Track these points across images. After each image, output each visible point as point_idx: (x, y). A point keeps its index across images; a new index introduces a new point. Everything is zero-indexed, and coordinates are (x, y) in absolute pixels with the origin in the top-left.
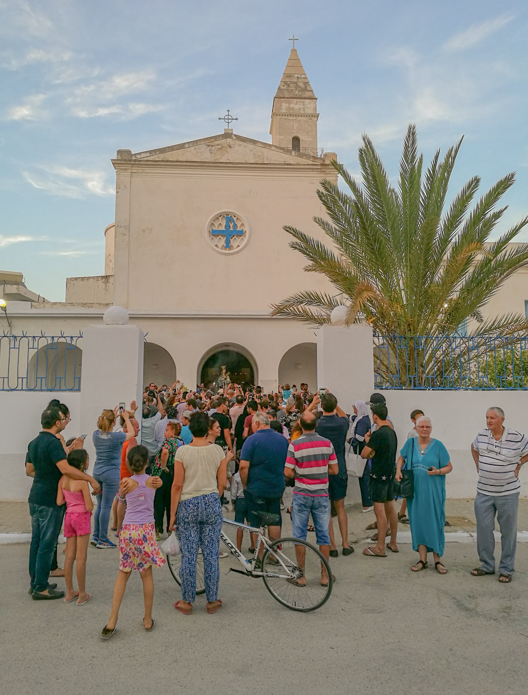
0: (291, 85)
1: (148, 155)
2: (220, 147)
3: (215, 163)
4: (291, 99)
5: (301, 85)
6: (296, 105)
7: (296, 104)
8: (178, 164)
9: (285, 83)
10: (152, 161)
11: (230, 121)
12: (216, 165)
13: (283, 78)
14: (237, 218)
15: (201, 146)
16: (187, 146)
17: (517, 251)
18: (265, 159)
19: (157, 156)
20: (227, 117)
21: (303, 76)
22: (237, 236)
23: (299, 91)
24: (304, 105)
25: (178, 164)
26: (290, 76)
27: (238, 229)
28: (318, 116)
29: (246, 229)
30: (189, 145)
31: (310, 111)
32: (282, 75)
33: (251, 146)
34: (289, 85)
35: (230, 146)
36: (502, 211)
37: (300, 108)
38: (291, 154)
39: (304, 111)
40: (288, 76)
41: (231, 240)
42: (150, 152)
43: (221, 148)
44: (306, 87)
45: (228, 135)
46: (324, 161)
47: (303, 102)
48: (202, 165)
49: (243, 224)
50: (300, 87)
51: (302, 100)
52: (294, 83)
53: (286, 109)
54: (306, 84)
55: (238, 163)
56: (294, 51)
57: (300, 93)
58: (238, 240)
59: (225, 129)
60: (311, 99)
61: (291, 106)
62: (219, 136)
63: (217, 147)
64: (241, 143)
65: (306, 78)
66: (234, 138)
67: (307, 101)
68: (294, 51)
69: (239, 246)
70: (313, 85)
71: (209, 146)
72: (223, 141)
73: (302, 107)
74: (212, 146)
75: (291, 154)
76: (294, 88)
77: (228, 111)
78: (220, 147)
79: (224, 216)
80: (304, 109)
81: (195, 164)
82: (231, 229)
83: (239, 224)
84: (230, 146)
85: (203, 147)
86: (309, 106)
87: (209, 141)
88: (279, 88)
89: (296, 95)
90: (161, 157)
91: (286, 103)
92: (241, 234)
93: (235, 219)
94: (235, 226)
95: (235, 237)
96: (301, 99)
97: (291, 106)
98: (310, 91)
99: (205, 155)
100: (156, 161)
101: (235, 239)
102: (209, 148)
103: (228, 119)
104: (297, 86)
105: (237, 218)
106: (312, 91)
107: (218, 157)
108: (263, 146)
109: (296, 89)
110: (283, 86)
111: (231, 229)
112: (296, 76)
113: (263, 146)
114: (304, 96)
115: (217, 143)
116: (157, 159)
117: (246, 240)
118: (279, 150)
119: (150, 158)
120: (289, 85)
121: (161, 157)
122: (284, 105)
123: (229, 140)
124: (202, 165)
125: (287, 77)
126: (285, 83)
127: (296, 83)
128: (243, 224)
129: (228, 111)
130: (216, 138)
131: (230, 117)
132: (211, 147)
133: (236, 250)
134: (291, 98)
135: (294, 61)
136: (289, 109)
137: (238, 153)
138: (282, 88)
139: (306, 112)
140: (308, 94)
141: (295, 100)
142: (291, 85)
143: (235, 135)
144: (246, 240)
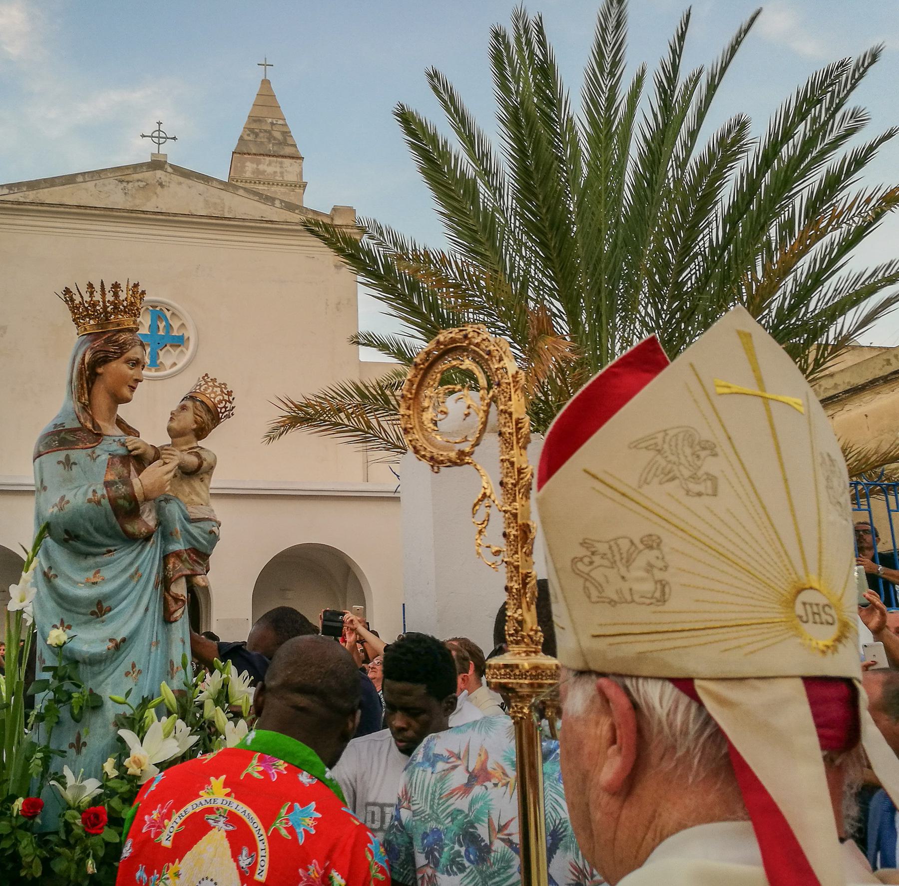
0: (261, 135)
1: (6, 191)
2: (142, 184)
3: (132, 211)
4: (261, 157)
5: (278, 135)
6: (269, 167)
7: (269, 164)
8: (62, 209)
9: (252, 131)
10: (12, 203)
11: (162, 140)
12: (134, 215)
13: (248, 123)
14: (173, 314)
15: (106, 181)
16: (80, 179)
17: (835, 290)
18: (226, 210)
19: (21, 194)
20: (156, 134)
21: (280, 122)
22: (171, 346)
23: (274, 144)
24: (281, 167)
25: (62, 209)
26: (259, 121)
27: (175, 333)
28: (305, 186)
29: (190, 333)
30: (84, 178)
31: (291, 178)
32: (247, 118)
33: (201, 186)
34: (257, 135)
35: (161, 185)
36: (872, 148)
37: (275, 172)
38: (273, 205)
39: (283, 177)
40: (254, 119)
41: (161, 353)
42: (10, 186)
43: (144, 187)
44: (285, 139)
45: (157, 164)
46: (332, 219)
47: (281, 163)
48: (108, 214)
49: (183, 324)
50: (275, 139)
51: (279, 159)
52: (265, 131)
53: (253, 173)
54: (286, 134)
55: (175, 215)
56: (266, 82)
57: (275, 148)
58: (175, 353)
59: (152, 154)
60: (293, 158)
61: (261, 167)
62: (141, 165)
63: (136, 184)
64: (181, 179)
65: (286, 125)
66: (170, 170)
67: (287, 161)
68: (266, 82)
69: (175, 364)
70: (298, 136)
71: (121, 181)
72: (147, 175)
73: (278, 170)
74: (128, 182)
75: (273, 205)
76: (266, 140)
77: (160, 123)
78: (142, 184)
79: (148, 309)
80: (282, 173)
81: (93, 212)
82: (161, 333)
83: (176, 324)
84: (161, 185)
85: (111, 184)
86: (290, 169)
87: (122, 173)
88: (241, 139)
89: (270, 150)
90: (31, 196)
91: (252, 163)
92: (179, 342)
93: (168, 314)
94: (169, 327)
95: (168, 347)
96: (276, 157)
97: (261, 167)
98: (292, 145)
99: (115, 197)
100: (19, 203)
101: (168, 351)
102: (122, 186)
103: (159, 137)
104: (271, 137)
105: (173, 314)
106: (295, 146)
107: (138, 202)
108: (222, 187)
109: (270, 141)
110: (249, 135)
111: (161, 333)
112: (270, 120)
113: (222, 187)
114: (282, 153)
115: (137, 176)
116: (21, 200)
117: (189, 353)
118: (251, 197)
119: (11, 198)
120: (257, 135)
121: (31, 196)
122: (250, 166)
123: (159, 173)
124: (108, 214)
125: (255, 121)
126: (252, 131)
127: (269, 132)
128: (183, 324)
129: (160, 123)
130: (137, 168)
131: (162, 135)
132: (125, 184)
133: (169, 371)
134: (260, 155)
135: (266, 97)
136: (257, 172)
137: (177, 197)
138: (246, 138)
139: (285, 178)
140: (288, 150)
141: (268, 159)
142: (261, 135)
143: (171, 165)
144: (189, 353)
